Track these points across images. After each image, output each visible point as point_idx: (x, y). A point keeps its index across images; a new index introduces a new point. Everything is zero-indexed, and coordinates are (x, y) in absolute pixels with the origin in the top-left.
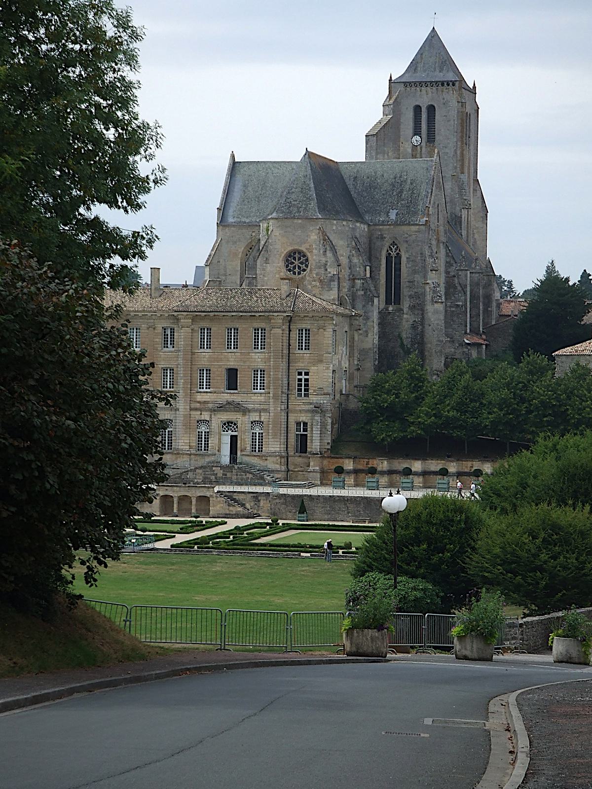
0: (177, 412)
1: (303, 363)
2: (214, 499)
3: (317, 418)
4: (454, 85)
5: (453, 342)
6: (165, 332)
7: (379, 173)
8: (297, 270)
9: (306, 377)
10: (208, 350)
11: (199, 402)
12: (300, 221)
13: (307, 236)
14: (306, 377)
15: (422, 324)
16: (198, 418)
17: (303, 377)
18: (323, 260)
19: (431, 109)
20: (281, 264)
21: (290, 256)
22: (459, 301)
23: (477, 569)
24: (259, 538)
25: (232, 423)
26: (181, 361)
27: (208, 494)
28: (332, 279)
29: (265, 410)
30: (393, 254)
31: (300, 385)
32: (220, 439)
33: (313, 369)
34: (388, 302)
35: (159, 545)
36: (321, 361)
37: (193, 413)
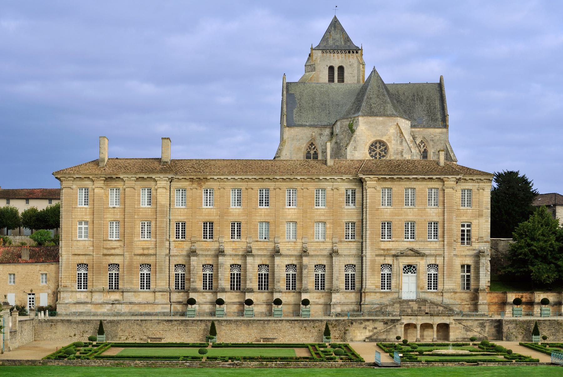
1: (466, 217)
4: (357, 52)
6: (347, 193)
8: (378, 156)
11: (384, 250)
12: (381, 119)
13: (387, 130)
14: (469, 228)
16: (382, 263)
18: (400, 148)
19: (341, 69)
20: (367, 151)
27: (447, 322)
33: (475, 222)
37: (377, 258)
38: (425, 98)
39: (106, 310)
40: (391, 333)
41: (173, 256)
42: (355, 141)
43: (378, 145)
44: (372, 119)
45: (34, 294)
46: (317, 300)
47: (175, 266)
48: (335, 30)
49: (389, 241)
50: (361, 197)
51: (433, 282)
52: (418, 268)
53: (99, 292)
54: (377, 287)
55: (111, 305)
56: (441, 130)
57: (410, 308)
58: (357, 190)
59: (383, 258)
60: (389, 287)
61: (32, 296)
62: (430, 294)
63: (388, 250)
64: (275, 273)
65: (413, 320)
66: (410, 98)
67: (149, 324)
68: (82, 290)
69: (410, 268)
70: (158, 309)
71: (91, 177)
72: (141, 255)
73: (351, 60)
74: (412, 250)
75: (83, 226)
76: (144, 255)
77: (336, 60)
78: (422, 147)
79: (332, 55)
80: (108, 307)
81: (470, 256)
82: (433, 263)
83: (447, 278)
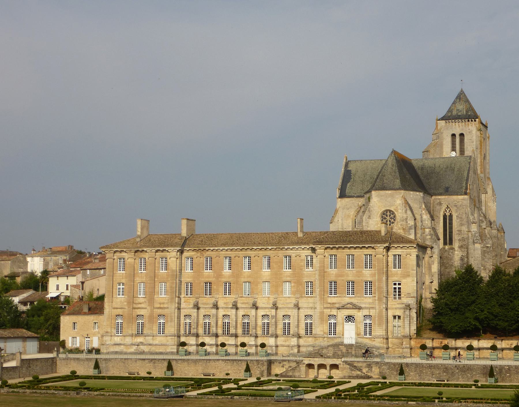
0: (316, 310)
1: (397, 277)
3: (407, 312)
5: (485, 269)
7: (437, 165)
8: (388, 223)
9: (399, 286)
10: (335, 270)
11: (330, 303)
12: (390, 192)
14: (399, 286)
15: (467, 258)
17: (397, 286)
18: (405, 216)
19: (462, 135)
20: (378, 219)
21: (384, 214)
22: (488, 243)
24: (375, 391)
25: (351, 317)
26: (317, 277)
28: (410, 228)
29: (372, 308)
30: (448, 214)
32: (343, 327)
33: (403, 281)
34: (445, 243)
35: (307, 396)
36: (409, 276)
37: (325, 310)
38: (456, 169)
39: (133, 350)
41: (183, 308)
42: (369, 211)
43: (388, 214)
44: (382, 192)
46: (284, 343)
48: (460, 101)
49: (312, 297)
51: (368, 329)
52: (355, 317)
53: (129, 336)
54: (325, 333)
55: (136, 346)
56: (463, 197)
57: (340, 350)
59: (330, 310)
60: (335, 333)
61: (88, 339)
62: (365, 339)
63: (333, 303)
65: (312, 361)
66: (444, 169)
67: (129, 362)
68: (119, 334)
69: (350, 318)
70: (169, 350)
71: (125, 250)
72: (158, 308)
73: (470, 127)
74: (351, 303)
75: (121, 287)
76: (161, 308)
77: (457, 128)
78: (448, 211)
79: (454, 124)
80: (135, 347)
81: (401, 308)
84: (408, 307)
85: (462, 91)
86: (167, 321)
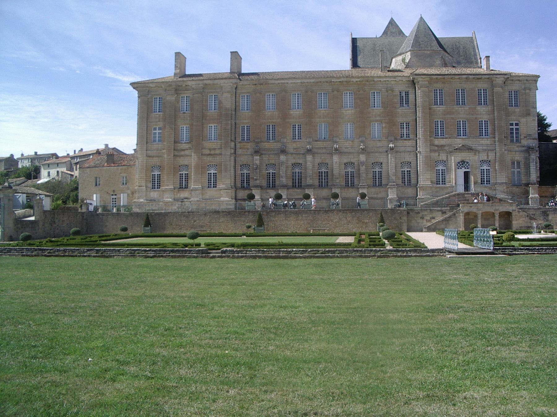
2: (517, 214)
11: (437, 146)
23: (128, 252)
31: (512, 133)
40: (450, 222)
45: (116, 195)
47: (241, 166)
49: (443, 138)
50: (414, 98)
58: (410, 91)
61: (114, 197)
64: (334, 170)
75: (157, 131)
82: (485, 158)
83: (500, 173)
84: (529, 149)
85: (392, 19)
86: (220, 172)
